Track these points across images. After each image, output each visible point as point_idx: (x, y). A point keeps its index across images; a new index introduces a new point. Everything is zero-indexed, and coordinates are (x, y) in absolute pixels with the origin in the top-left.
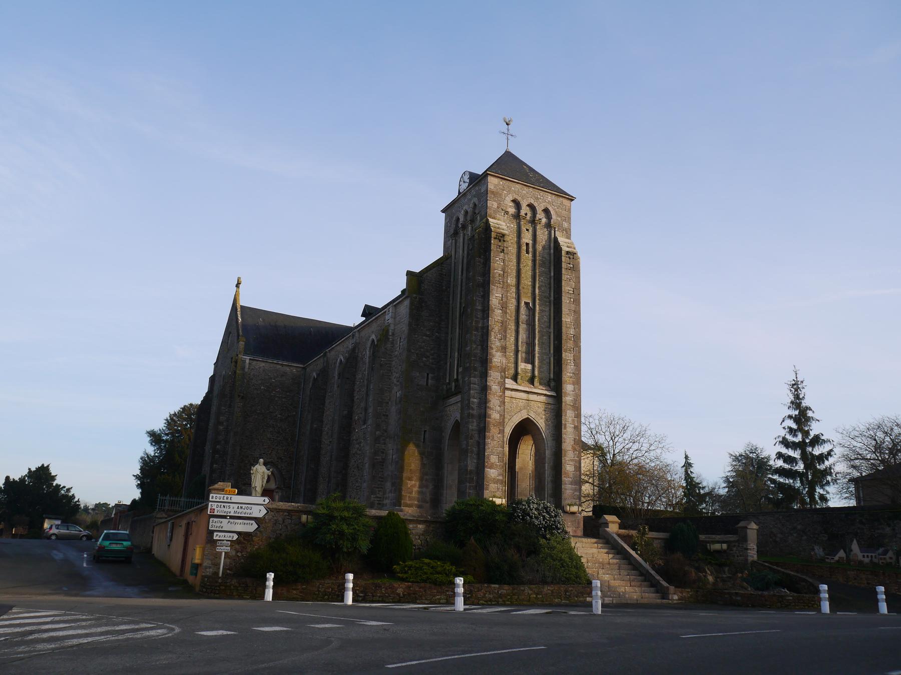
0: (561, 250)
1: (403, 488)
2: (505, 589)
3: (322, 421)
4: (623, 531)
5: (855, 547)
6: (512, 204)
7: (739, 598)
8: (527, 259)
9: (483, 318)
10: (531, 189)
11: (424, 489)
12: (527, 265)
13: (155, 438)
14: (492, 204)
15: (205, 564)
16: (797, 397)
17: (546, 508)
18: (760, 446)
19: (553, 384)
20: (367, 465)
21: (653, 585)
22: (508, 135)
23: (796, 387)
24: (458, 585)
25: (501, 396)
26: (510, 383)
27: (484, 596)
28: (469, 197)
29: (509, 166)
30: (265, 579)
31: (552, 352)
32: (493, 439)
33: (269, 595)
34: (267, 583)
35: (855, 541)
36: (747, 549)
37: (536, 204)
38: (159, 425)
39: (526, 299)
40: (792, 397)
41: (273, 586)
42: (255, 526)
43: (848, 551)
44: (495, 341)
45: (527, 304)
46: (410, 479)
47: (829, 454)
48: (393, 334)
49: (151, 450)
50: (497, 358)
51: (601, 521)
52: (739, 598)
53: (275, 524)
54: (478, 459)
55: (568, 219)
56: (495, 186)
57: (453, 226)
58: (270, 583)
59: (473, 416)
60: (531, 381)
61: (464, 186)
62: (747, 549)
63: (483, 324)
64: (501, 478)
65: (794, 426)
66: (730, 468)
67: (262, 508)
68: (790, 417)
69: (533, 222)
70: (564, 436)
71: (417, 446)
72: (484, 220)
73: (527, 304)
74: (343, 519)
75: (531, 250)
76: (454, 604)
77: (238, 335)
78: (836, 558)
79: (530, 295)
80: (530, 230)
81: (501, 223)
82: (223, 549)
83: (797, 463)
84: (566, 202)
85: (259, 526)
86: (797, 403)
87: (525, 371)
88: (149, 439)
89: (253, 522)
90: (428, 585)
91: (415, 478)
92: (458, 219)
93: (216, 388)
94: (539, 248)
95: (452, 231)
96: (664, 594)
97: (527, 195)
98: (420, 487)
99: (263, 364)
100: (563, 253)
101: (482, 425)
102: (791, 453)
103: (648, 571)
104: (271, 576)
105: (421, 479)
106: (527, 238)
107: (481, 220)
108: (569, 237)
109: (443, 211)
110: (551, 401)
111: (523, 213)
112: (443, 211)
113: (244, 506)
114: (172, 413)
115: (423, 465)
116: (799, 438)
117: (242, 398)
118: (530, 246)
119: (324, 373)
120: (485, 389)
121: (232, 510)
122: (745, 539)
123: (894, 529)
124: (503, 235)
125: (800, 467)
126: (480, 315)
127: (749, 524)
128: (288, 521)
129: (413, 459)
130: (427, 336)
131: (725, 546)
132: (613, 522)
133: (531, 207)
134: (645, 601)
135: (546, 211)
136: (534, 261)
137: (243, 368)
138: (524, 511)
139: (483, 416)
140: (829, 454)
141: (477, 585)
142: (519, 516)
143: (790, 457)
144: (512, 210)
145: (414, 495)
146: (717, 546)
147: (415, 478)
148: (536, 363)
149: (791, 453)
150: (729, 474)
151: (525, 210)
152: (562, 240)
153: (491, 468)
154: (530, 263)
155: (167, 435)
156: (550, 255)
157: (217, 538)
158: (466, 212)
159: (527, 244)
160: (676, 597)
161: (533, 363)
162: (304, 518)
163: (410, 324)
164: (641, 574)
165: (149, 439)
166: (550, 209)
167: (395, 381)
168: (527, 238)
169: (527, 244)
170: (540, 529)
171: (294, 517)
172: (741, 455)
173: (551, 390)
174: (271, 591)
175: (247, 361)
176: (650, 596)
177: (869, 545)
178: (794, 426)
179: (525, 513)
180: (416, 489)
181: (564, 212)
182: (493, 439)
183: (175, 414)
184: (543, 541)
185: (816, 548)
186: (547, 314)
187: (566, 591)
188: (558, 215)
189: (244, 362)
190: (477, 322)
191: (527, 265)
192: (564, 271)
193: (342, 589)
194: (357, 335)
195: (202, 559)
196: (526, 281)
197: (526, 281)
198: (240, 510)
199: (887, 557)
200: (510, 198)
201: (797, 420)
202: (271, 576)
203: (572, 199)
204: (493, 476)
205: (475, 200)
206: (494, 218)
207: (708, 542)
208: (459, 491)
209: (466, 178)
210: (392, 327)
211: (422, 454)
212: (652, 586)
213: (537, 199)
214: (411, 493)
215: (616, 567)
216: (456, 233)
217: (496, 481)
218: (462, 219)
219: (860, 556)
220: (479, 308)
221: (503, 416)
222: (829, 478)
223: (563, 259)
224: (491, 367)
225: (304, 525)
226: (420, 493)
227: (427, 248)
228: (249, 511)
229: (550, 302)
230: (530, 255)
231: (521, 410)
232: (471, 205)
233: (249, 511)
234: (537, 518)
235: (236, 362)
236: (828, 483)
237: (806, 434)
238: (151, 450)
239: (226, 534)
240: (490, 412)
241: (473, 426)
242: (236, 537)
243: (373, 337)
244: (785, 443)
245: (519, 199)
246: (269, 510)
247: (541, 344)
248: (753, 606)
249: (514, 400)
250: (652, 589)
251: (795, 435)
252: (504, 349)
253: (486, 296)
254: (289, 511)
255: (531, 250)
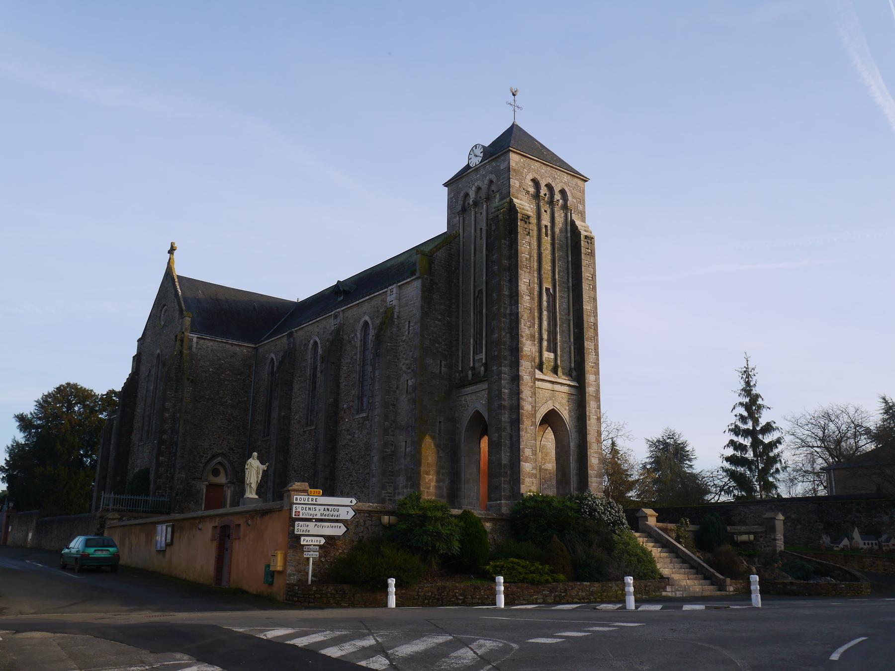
0: (580, 233)
1: (422, 483)
2: (596, 587)
3: (290, 409)
4: (660, 524)
5: (856, 534)
6: (531, 183)
7: (794, 588)
8: (547, 241)
9: (511, 305)
10: (549, 168)
11: (441, 484)
12: (546, 249)
13: (24, 422)
14: (514, 183)
15: (289, 571)
16: (748, 383)
17: (609, 503)
18: (678, 431)
19: (574, 374)
20: (376, 459)
21: (707, 577)
22: (515, 107)
23: (747, 374)
24: (629, 584)
25: (532, 387)
26: (539, 374)
27: (577, 595)
28: (483, 172)
29: (511, 140)
30: (386, 586)
31: (572, 340)
32: (526, 432)
33: (392, 601)
35: (856, 529)
36: (775, 540)
37: (554, 185)
38: (29, 408)
39: (547, 285)
40: (742, 385)
42: (344, 529)
43: (851, 539)
44: (526, 329)
45: (547, 289)
46: (428, 473)
47: (779, 441)
48: (398, 317)
49: (21, 437)
50: (528, 348)
51: (638, 515)
52: (794, 588)
53: (357, 526)
54: (512, 452)
55: (582, 201)
56: (517, 163)
57: (460, 202)
58: (392, 589)
59: (504, 407)
60: (555, 371)
61: (475, 161)
62: (775, 540)
63: (511, 310)
64: (534, 472)
65: (745, 414)
66: (648, 455)
67: (349, 509)
68: (741, 404)
69: (551, 202)
70: (588, 428)
71: (433, 438)
72: (508, 199)
73: (547, 289)
74: (437, 519)
75: (549, 232)
77: (181, 311)
78: (841, 546)
79: (550, 280)
81: (524, 204)
82: (312, 555)
83: (747, 451)
84: (580, 182)
85: (348, 529)
86: (747, 390)
87: (548, 360)
88: (18, 424)
89: (341, 525)
90: (525, 585)
91: (432, 472)
92: (467, 195)
93: (143, 369)
94: (557, 230)
95: (459, 208)
96: (721, 586)
97: (546, 175)
98: (437, 481)
99: (211, 343)
100: (582, 238)
101: (514, 417)
102: (740, 440)
103: (700, 564)
104: (392, 582)
105: (438, 473)
106: (546, 221)
107: (501, 199)
108: (584, 220)
109: (446, 185)
110: (573, 391)
111: (542, 194)
112: (446, 185)
113: (330, 508)
114: (46, 393)
115: (439, 458)
116: (750, 425)
117: (192, 381)
118: (549, 228)
119: (290, 357)
120: (516, 379)
121: (318, 513)
122: (773, 529)
123: (891, 517)
124: (529, 217)
125: (750, 455)
126: (507, 301)
127: (777, 515)
128: (369, 523)
129: (429, 452)
130: (439, 320)
131: (752, 537)
132: (652, 516)
133: (549, 187)
134: (706, 594)
135: (563, 192)
136: (553, 244)
137: (190, 348)
138: (590, 507)
139: (517, 407)
140: (779, 441)
141: (570, 584)
142: (585, 512)
143: (741, 444)
144: (532, 190)
145: (432, 490)
146: (744, 538)
147: (432, 472)
148: (559, 353)
149: (740, 440)
150: (647, 460)
151: (544, 191)
152: (578, 223)
154: (549, 247)
155: (40, 419)
156: (567, 238)
157: (305, 543)
158: (479, 189)
159: (546, 226)
160: (732, 589)
161: (555, 352)
162: (385, 519)
163: (422, 307)
164: (692, 567)
165: (18, 424)
166: (567, 190)
167: (404, 368)
168: (546, 221)
169: (546, 226)
170: (609, 524)
171: (374, 518)
172: (658, 441)
173: (573, 380)
174: (502, 596)
175: (195, 340)
176: (710, 590)
177: (870, 532)
178: (745, 414)
179: (593, 510)
180: (433, 484)
181: (579, 194)
183: (49, 395)
184: (615, 537)
185: (824, 537)
186: (566, 300)
187: (646, 586)
188: (574, 197)
189: (191, 340)
190: (505, 308)
191: (546, 249)
192: (583, 257)
193: (494, 593)
194: (341, 315)
195: (285, 565)
196: (547, 266)
197: (547, 266)
198: (327, 513)
199: (890, 544)
200: (530, 177)
201: (748, 407)
202: (392, 582)
203: (585, 180)
205: (493, 177)
206: (517, 198)
207: (735, 533)
208: (490, 486)
209: (479, 152)
210: (397, 310)
211: (437, 446)
212: (705, 578)
213: (554, 178)
214: (429, 488)
215: (668, 560)
216: (464, 210)
218: (472, 195)
219: (861, 545)
220: (507, 293)
221: (534, 407)
222: (778, 465)
223: (582, 243)
225: (384, 526)
226: (437, 487)
227: (428, 221)
228: (336, 513)
229: (568, 288)
230: (549, 238)
232: (486, 182)
233: (336, 513)
234: (605, 514)
235: (182, 341)
236: (777, 471)
237: (756, 421)
238: (21, 437)
239: (313, 538)
240: (523, 403)
241: (505, 417)
242: (323, 541)
243: (367, 318)
244: (736, 431)
245: (539, 178)
246: (357, 511)
247: (562, 332)
248: (810, 595)
249: (544, 392)
250: (708, 582)
251: (746, 423)
252: (532, 337)
253: (514, 281)
254: (369, 512)
255: (549, 232)
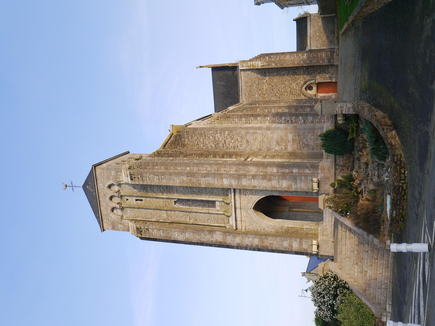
10: (100, 199)
32: (272, 244)
34: (404, 251)
41: (407, 242)
76: (427, 126)
80: (128, 198)
153: (292, 246)
169: (137, 200)
182: (272, 244)
204: (297, 245)
217: (301, 244)
224: (225, 243)
231: (248, 214)
